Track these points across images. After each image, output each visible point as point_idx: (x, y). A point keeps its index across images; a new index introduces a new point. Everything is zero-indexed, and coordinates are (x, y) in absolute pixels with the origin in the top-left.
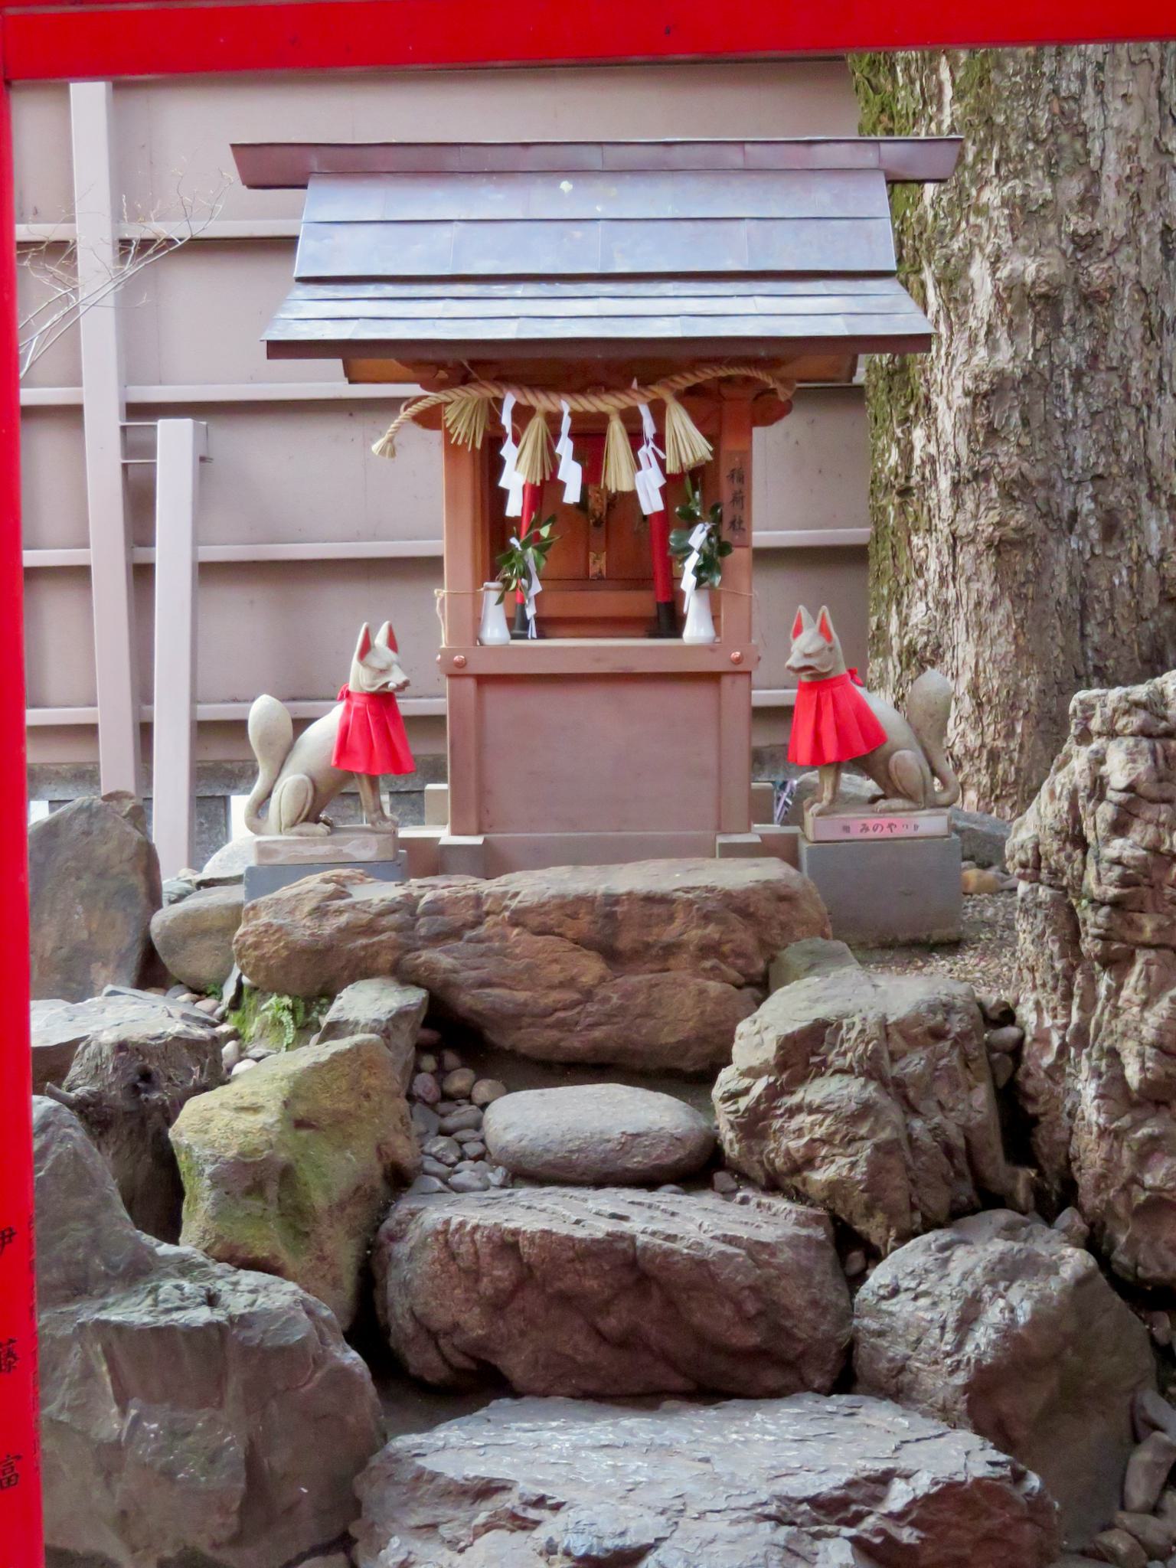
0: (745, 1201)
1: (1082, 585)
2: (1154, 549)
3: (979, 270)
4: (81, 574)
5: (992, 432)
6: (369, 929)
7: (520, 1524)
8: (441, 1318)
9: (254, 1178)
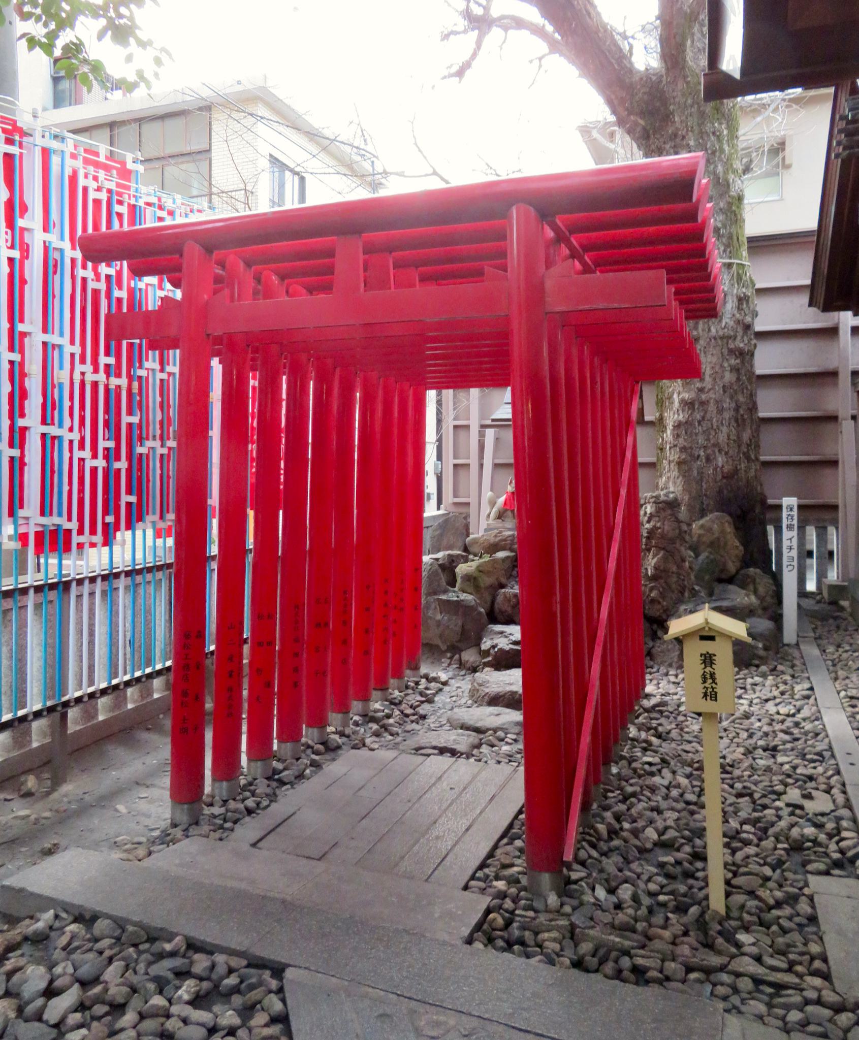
0: (6, 233)
1: (700, 473)
2: (720, 465)
3: (675, 396)
4: (468, 465)
5: (678, 436)
6: (505, 540)
7: (506, 637)
8: (503, 609)
9: (468, 578)
